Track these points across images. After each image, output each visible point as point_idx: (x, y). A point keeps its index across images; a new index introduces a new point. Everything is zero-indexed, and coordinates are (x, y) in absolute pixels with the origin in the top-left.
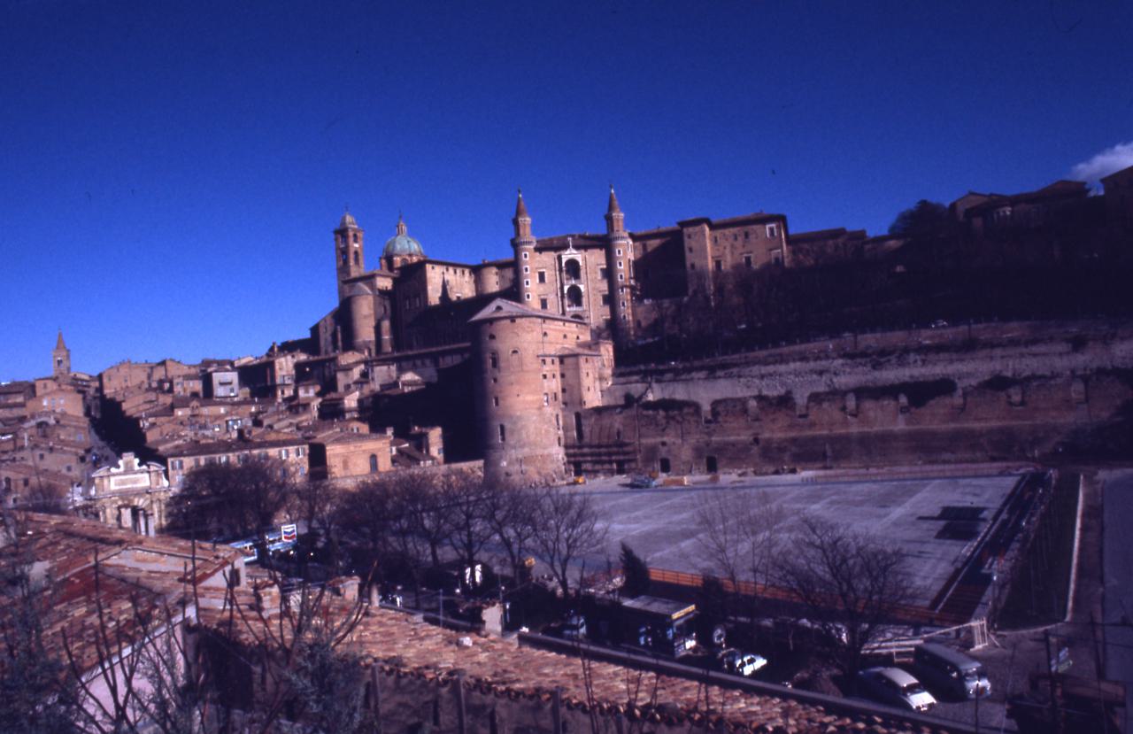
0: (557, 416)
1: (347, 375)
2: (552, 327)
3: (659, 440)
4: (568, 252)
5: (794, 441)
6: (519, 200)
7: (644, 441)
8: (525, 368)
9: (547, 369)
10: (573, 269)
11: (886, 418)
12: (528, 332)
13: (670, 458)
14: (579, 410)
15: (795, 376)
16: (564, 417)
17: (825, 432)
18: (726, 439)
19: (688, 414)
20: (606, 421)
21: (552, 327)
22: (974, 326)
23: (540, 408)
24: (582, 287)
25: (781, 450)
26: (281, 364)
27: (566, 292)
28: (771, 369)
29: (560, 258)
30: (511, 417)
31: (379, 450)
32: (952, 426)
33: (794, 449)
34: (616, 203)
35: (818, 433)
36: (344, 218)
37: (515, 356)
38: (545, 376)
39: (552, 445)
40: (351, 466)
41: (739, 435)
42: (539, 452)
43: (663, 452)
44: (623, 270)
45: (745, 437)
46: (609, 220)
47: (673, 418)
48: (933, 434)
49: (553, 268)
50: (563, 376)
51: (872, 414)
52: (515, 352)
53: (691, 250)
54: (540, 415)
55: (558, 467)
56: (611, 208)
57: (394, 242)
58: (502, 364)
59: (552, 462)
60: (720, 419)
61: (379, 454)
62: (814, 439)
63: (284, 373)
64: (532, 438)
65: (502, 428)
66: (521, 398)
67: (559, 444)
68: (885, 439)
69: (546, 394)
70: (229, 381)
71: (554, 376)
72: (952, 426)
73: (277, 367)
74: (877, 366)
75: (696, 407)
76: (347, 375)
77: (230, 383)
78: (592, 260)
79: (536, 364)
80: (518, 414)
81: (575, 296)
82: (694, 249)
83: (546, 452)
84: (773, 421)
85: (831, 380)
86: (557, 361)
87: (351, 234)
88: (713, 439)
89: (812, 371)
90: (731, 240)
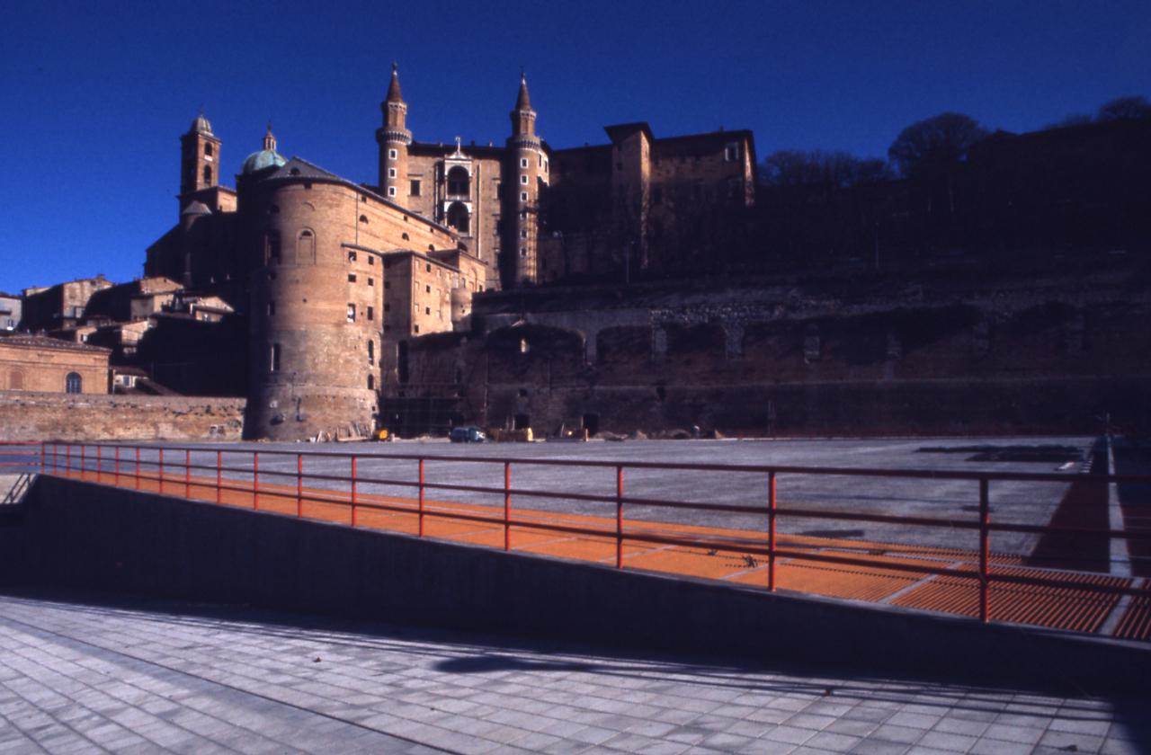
1: (145, 305)
2: (377, 212)
3: (518, 386)
4: (453, 157)
6: (393, 76)
8: (319, 260)
10: (459, 181)
12: (331, 206)
15: (728, 307)
16: (384, 348)
21: (377, 212)
23: (340, 325)
24: (470, 207)
26: (73, 290)
27: (446, 209)
29: (441, 166)
30: (292, 333)
31: (89, 367)
34: (527, 98)
36: (195, 124)
38: (352, 279)
39: (355, 384)
40: (26, 380)
42: (331, 390)
44: (529, 190)
45: (645, 387)
46: (516, 120)
49: (431, 176)
53: (620, 166)
54: (338, 335)
55: (362, 418)
56: (520, 104)
57: (256, 157)
59: (352, 408)
61: (85, 375)
63: (77, 303)
64: (321, 368)
66: (309, 305)
67: (370, 387)
69: (353, 306)
70: (7, 309)
73: (67, 294)
75: (574, 343)
76: (145, 305)
77: (8, 313)
78: (484, 174)
79: (340, 257)
83: (343, 393)
87: (202, 142)
88: (597, 387)
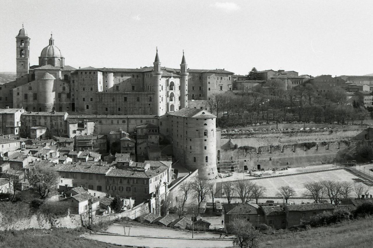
5: (280, 159)
11: (301, 153)
13: (247, 165)
17: (288, 157)
18: (263, 159)
19: (252, 151)
22: (306, 124)
25: (277, 162)
28: (264, 135)
32: (315, 155)
33: (280, 162)
35: (286, 157)
41: (266, 158)
47: (249, 152)
48: (311, 157)
51: (298, 152)
52: (212, 130)
53: (209, 83)
60: (261, 153)
62: (285, 159)
65: (207, 157)
68: (301, 158)
72: (315, 155)
74: (291, 136)
80: (212, 152)
81: (324, 144)
82: (210, 83)
84: (275, 153)
85: (280, 140)
89: (275, 137)
90: (216, 79)
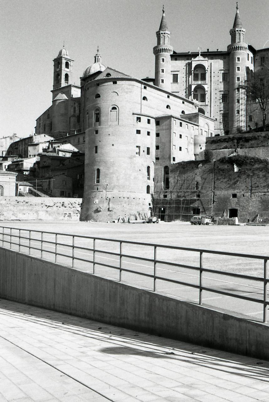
0: (148, 168)
3: (231, 192)
7: (218, 193)
9: (143, 125)
14: (167, 164)
19: (257, 169)
20: (189, 175)
24: (206, 87)
29: (190, 65)
37: (114, 112)
38: (138, 132)
43: (233, 203)
44: (241, 75)
50: (158, 135)
58: (103, 119)
65: (98, 170)
71: (148, 133)
76: (35, 149)
78: (216, 66)
86: (153, 121)
